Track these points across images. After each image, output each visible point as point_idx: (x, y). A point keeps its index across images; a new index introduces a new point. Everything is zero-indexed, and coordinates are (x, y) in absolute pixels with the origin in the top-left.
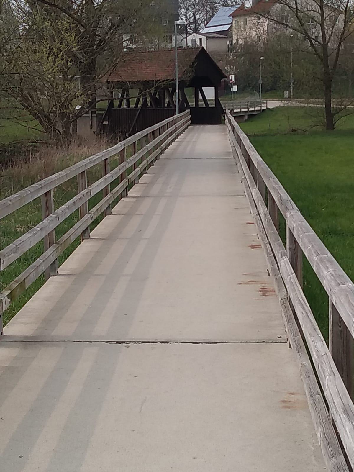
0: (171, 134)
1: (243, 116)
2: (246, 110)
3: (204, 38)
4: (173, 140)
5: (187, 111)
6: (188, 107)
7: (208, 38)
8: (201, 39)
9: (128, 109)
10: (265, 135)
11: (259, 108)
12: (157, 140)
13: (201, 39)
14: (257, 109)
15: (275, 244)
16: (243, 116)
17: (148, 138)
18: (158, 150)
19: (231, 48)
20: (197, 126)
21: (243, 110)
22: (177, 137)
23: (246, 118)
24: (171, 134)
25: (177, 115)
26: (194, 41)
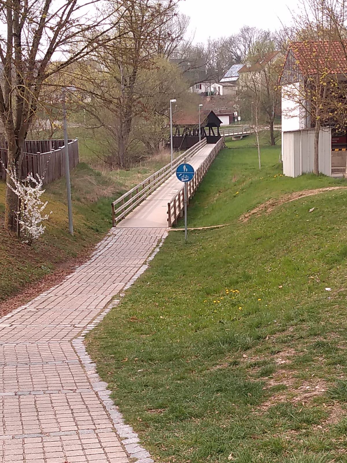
0: (197, 149)
1: (240, 137)
2: (241, 133)
3: (221, 87)
4: (198, 151)
5: (205, 138)
6: (206, 136)
7: (223, 86)
8: (219, 87)
9: (179, 137)
10: (243, 148)
11: (250, 132)
12: (192, 151)
13: (219, 87)
14: (248, 132)
15: (145, 117)
16: (240, 137)
17: (190, 151)
18: (192, 154)
19: (238, 93)
20: (209, 145)
21: (239, 133)
22: (199, 150)
23: (241, 137)
24: (197, 149)
25: (200, 141)
26: (215, 88)
